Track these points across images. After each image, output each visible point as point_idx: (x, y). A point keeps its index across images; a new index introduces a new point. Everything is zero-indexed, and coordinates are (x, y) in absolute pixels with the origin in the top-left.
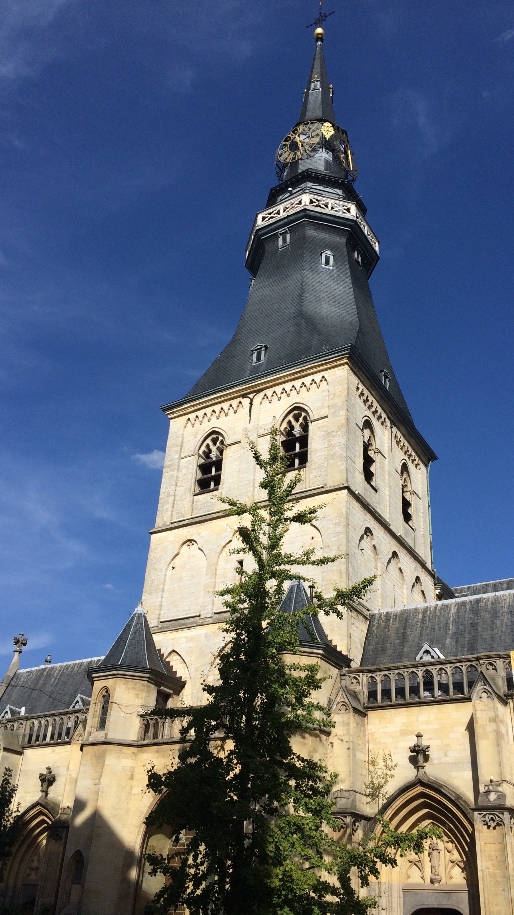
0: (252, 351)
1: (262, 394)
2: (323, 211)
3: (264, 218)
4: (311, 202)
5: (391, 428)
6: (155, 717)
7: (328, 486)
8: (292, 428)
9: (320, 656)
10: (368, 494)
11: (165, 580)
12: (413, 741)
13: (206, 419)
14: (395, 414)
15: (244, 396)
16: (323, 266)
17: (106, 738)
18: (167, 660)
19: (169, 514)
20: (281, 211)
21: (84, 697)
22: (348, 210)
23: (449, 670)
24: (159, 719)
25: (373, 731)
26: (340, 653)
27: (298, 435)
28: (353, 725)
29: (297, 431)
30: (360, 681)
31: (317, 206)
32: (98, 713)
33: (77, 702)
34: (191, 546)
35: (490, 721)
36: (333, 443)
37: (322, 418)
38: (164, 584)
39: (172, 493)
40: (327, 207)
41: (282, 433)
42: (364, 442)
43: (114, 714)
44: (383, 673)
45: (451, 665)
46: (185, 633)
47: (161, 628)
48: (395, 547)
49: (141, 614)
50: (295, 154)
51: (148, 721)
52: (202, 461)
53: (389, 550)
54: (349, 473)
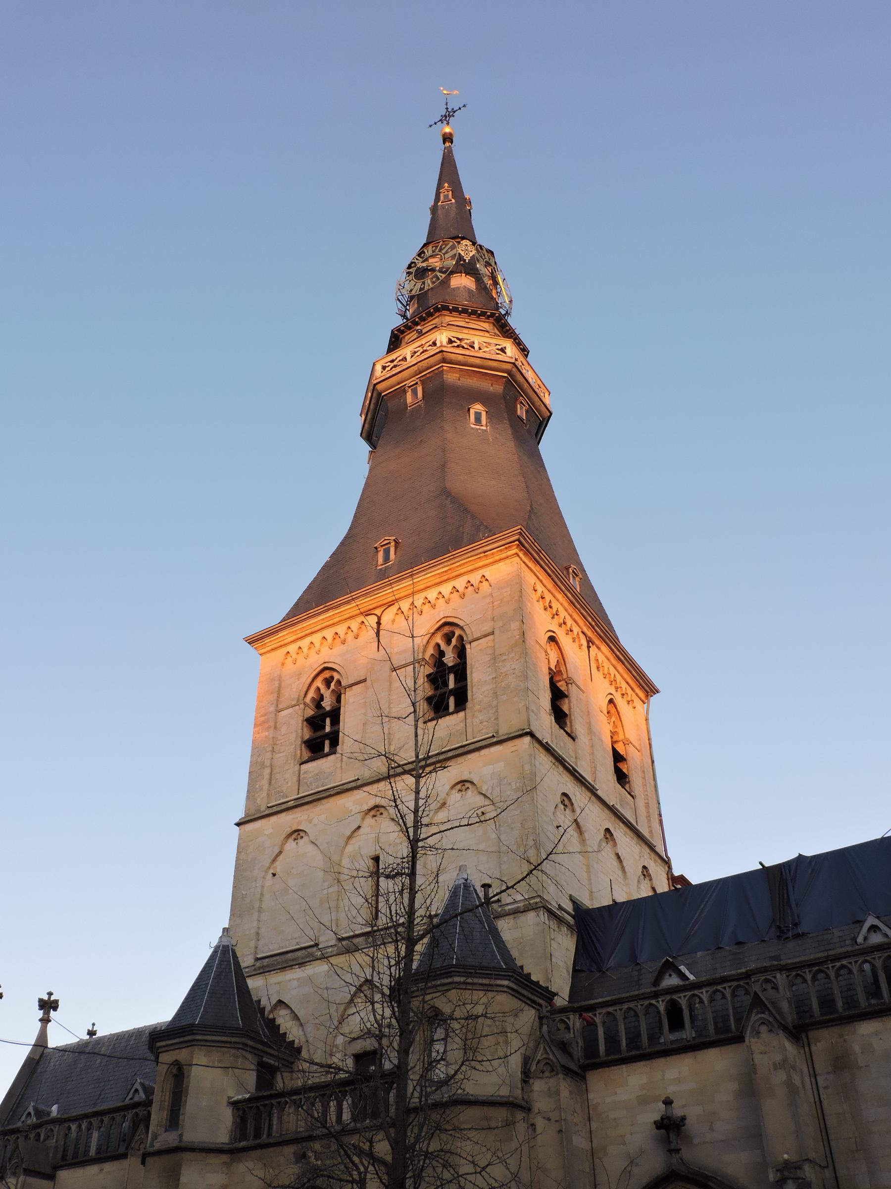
0: (376, 548)
1: (394, 609)
2: (467, 353)
3: (384, 368)
4: (450, 341)
5: (589, 647)
6: (255, 1105)
7: (501, 733)
8: (442, 654)
9: (505, 989)
10: (562, 744)
11: (262, 894)
12: (657, 1111)
13: (313, 651)
14: (593, 627)
15: (367, 614)
16: (473, 426)
17: (181, 1141)
18: (271, 1016)
19: (264, 794)
20: (408, 357)
21: (147, 1083)
22: (503, 350)
23: (705, 997)
24: (261, 1108)
25: (594, 1102)
26: (537, 984)
27: (450, 664)
28: (565, 1093)
29: (450, 659)
30: (571, 1025)
31: (458, 346)
32: (166, 1104)
33: (136, 1090)
34: (299, 841)
35: (775, 1068)
36: (503, 670)
37: (485, 636)
38: (261, 900)
39: (267, 763)
40: (473, 348)
41: (427, 663)
42: (550, 669)
43: (193, 1104)
44: (604, 1010)
45: (708, 989)
46: (297, 973)
47: (259, 968)
48: (607, 821)
49: (228, 946)
50: (424, 283)
51: (244, 1111)
52: (310, 713)
53: (599, 827)
54: (531, 713)
